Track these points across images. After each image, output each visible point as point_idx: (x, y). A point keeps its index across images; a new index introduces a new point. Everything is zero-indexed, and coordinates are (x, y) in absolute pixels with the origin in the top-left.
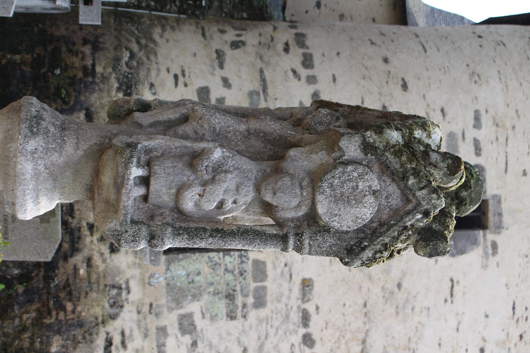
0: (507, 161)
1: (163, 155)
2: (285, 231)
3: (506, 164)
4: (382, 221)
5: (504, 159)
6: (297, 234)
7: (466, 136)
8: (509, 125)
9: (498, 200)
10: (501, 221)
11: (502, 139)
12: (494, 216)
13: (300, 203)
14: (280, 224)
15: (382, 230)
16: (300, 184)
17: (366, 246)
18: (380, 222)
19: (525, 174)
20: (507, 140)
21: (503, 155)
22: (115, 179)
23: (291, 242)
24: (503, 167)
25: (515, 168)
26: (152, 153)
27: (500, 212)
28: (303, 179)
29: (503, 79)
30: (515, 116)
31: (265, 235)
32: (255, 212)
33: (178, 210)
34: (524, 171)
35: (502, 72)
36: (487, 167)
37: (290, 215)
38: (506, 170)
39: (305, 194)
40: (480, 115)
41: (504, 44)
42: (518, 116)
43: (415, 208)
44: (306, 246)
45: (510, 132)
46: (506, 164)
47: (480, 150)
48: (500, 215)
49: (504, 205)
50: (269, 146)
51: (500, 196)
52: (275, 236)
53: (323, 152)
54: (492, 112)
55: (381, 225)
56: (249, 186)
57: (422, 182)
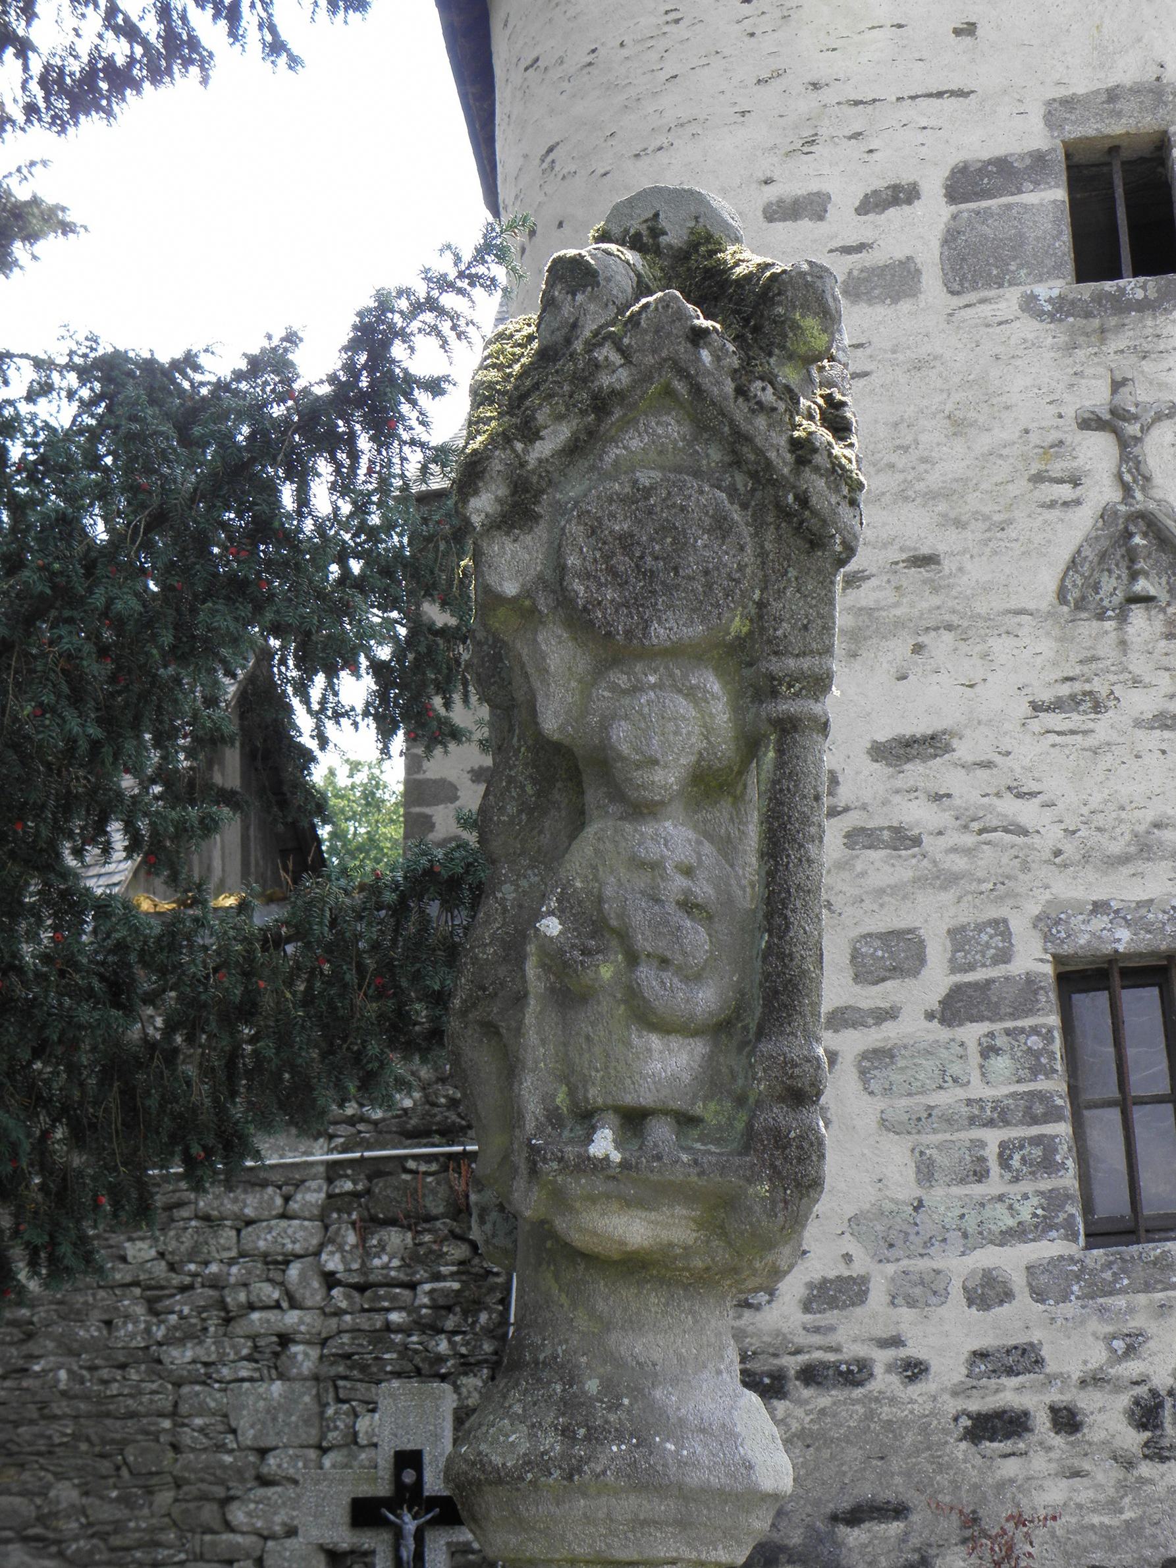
0: (930, 95)
1: (565, 1078)
2: (765, 727)
3: (940, 95)
4: (727, 459)
5: (923, 103)
6: (774, 694)
7: (852, 241)
8: (807, 104)
9: (1060, 109)
10: (1137, 90)
11: (857, 120)
12: (1119, 114)
13: (680, 691)
14: (751, 746)
15: (752, 457)
16: (625, 692)
17: (796, 497)
18: (730, 465)
19: (968, 30)
20: (857, 103)
21: (908, 111)
22: (628, 1205)
23: (786, 707)
24: (948, 103)
25: (952, 65)
26: (558, 1108)
27: (1104, 97)
28: (614, 688)
29: (662, 140)
30: (777, 85)
31: (779, 782)
32: (732, 820)
33: (721, 1029)
34: (957, 32)
35: (637, 148)
36: (955, 158)
37: (721, 713)
38: (961, 94)
39: (652, 679)
40: (781, 201)
41: (551, 150)
42: (778, 74)
43: (682, 373)
44: (806, 663)
45: (829, 96)
46: (940, 95)
47: (896, 188)
48: (1113, 95)
49: (1080, 86)
50: (556, 796)
51: (1049, 103)
52: (780, 752)
53: (540, 638)
54: (766, 165)
55: (737, 462)
56: (642, 834)
57: (606, 358)
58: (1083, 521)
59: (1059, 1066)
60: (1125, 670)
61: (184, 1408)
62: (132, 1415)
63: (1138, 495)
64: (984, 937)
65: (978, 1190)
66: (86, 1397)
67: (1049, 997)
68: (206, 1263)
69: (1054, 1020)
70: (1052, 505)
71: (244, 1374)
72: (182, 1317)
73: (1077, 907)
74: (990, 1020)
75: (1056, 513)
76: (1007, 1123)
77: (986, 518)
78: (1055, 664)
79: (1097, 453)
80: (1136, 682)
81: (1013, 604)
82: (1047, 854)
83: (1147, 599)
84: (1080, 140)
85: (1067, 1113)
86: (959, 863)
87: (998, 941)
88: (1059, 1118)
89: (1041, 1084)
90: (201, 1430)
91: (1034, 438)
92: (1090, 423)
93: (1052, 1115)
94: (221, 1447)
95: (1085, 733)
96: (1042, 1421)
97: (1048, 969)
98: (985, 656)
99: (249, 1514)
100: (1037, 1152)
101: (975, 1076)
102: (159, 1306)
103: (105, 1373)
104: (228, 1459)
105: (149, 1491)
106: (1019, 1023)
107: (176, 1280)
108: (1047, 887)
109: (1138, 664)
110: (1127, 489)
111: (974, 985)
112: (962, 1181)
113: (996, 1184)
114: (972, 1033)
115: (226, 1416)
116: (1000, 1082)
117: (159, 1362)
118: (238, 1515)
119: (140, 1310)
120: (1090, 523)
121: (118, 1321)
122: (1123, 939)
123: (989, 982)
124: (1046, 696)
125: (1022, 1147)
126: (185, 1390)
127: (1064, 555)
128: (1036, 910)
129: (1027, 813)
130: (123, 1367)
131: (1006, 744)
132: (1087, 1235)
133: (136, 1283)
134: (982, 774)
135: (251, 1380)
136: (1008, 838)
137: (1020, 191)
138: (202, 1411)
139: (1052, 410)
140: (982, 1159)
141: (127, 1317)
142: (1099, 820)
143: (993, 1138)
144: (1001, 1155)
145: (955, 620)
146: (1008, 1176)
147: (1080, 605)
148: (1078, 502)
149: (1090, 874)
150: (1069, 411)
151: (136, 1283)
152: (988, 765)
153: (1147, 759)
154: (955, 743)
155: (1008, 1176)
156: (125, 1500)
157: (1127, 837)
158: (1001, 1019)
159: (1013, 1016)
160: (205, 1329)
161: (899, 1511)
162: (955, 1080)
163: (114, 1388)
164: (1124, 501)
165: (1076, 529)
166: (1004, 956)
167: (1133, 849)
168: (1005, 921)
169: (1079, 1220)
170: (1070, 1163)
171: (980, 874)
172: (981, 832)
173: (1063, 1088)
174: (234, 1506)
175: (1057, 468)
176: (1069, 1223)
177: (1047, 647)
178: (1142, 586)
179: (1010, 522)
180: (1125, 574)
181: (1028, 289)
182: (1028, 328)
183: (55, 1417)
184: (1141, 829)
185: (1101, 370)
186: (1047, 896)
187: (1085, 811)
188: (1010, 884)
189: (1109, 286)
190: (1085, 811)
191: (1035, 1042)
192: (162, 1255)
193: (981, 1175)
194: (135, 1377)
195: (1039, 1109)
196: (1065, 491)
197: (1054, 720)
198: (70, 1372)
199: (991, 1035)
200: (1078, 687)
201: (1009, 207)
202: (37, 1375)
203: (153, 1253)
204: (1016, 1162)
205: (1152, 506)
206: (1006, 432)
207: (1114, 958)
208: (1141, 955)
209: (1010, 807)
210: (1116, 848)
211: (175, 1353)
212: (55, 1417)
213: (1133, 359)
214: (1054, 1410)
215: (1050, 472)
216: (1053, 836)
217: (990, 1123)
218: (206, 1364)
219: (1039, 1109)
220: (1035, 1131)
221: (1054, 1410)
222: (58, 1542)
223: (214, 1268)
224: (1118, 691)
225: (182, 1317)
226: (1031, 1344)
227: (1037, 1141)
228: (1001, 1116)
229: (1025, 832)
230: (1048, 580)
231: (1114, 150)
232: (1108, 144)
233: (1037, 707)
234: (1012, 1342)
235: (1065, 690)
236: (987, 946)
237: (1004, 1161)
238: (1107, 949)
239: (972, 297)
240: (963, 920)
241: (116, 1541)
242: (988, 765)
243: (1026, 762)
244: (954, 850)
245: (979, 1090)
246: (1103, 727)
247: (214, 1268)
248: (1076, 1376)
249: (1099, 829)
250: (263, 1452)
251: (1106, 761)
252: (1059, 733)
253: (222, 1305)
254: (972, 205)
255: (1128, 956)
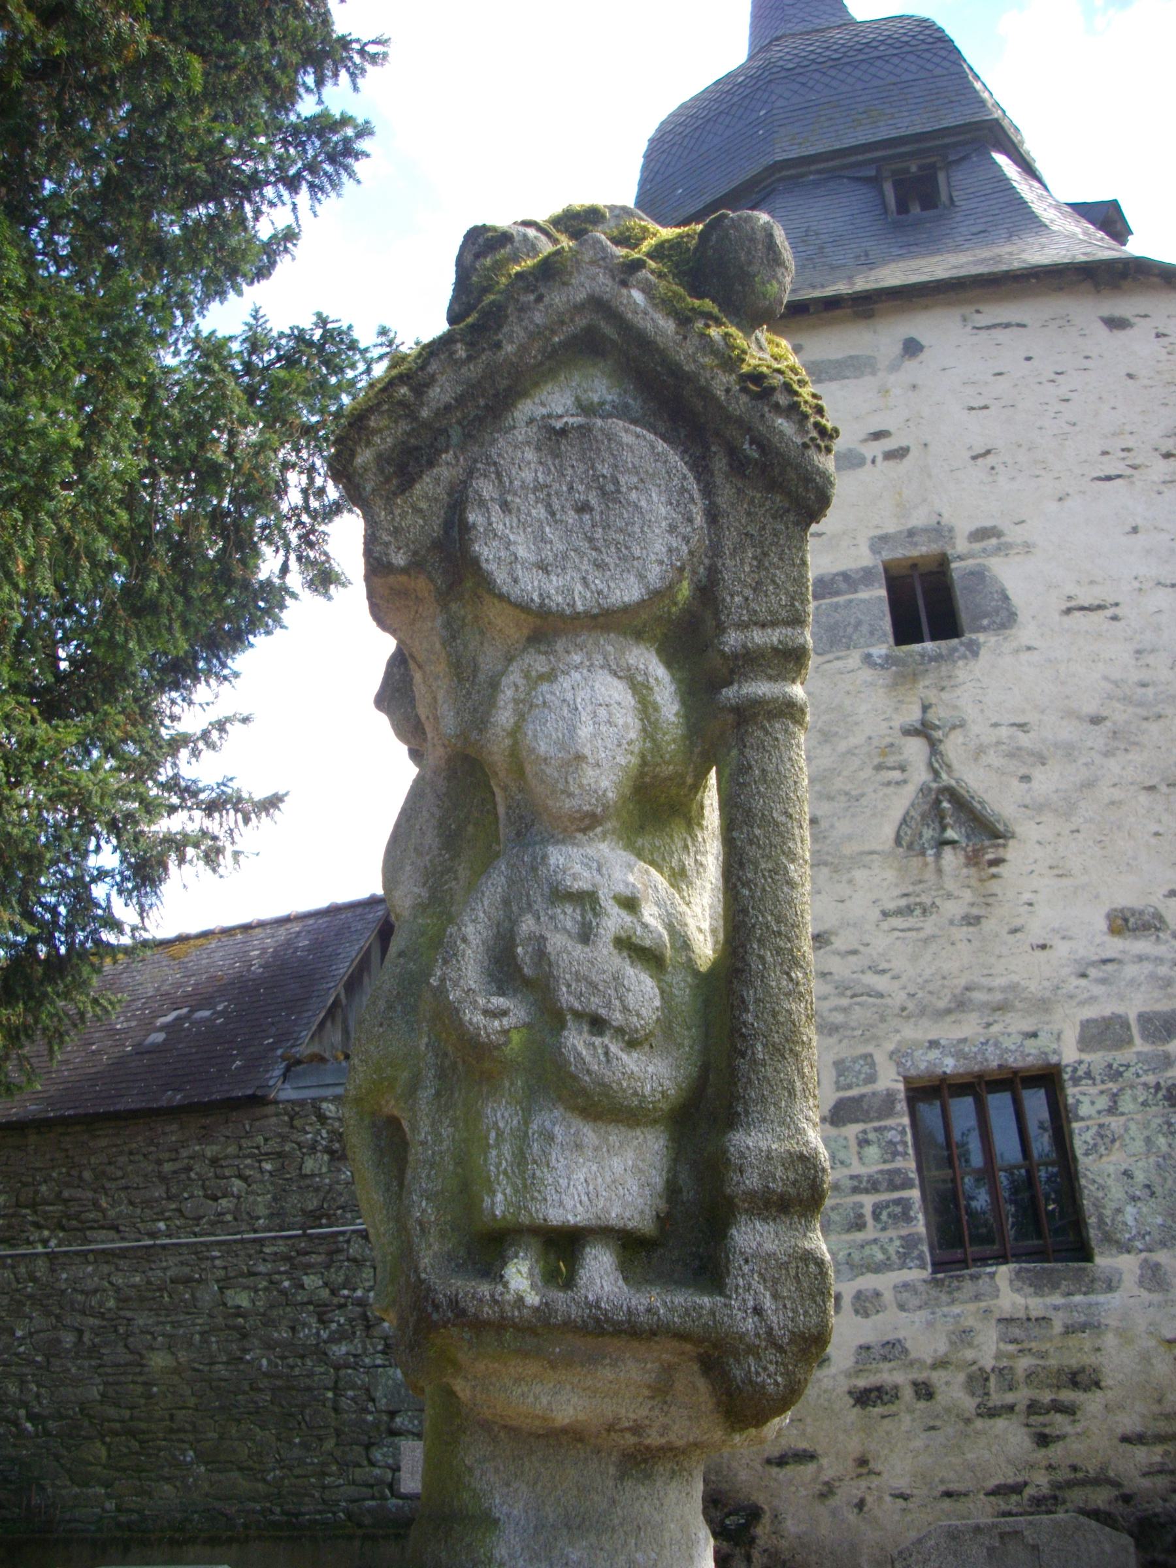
9: (880, 541)
10: (925, 530)
12: (916, 544)
48: (911, 533)
49: (891, 528)
51: (872, 538)
58: (909, 792)
59: (911, 1151)
60: (942, 888)
61: (341, 1384)
62: (309, 1389)
63: (944, 776)
64: (857, 1067)
65: (859, 1236)
66: (278, 1376)
67: (902, 1106)
68: (354, 1290)
69: (906, 1120)
70: (889, 784)
71: (379, 1362)
72: (339, 1325)
73: (916, 1044)
74: (864, 1121)
75: (891, 789)
76: (877, 1190)
77: (847, 794)
78: (897, 885)
79: (915, 749)
80: (949, 896)
81: (867, 848)
82: (897, 1011)
83: (952, 843)
84: (893, 560)
85: (917, 1182)
86: (839, 1018)
87: (866, 1069)
88: (912, 1186)
89: (899, 1163)
90: (353, 1399)
91: (875, 743)
92: (909, 732)
93: (907, 1184)
94: (366, 1410)
95: (918, 929)
96: (908, 1393)
97: (901, 1086)
98: (850, 881)
99: (384, 1455)
100: (898, 1210)
101: (855, 1161)
102: (326, 1317)
103: (291, 1361)
104: (370, 1418)
105: (320, 1439)
106: (882, 1123)
107: (335, 1300)
108: (898, 1031)
109: (950, 885)
110: (936, 774)
111: (852, 1099)
112: (848, 1231)
113: (870, 1232)
114: (852, 1130)
115: (368, 1390)
116: (872, 1163)
117: (326, 1354)
118: (377, 1455)
119: (313, 1321)
120: (913, 795)
121: (299, 1327)
122: (949, 1065)
123: (863, 1096)
124: (891, 906)
125: (887, 1206)
126: (342, 1372)
127: (897, 814)
128: (891, 1047)
129: (880, 983)
130: (303, 1357)
131: (867, 938)
132: (934, 1264)
133: (310, 1303)
134: (853, 959)
135: (384, 1366)
136: (871, 1000)
137: (856, 591)
138: (353, 1387)
139: (885, 724)
140: (861, 1216)
141: (304, 1325)
142: (930, 987)
143: (868, 1201)
144: (874, 1212)
145: (830, 859)
146: (879, 1226)
147: (910, 846)
148: (905, 782)
149: (925, 1022)
150: (896, 724)
151: (310, 1303)
152: (854, 952)
153: (959, 946)
154: (833, 939)
155: (879, 1226)
156: (305, 1446)
157: (949, 996)
158: (871, 1121)
159: (879, 1118)
160: (354, 1333)
161: (807, 1457)
162: (842, 1163)
163: (297, 1371)
164: (935, 781)
165: (901, 801)
166: (871, 1079)
167: (953, 1005)
168: (871, 1055)
169: (928, 1254)
170: (920, 1216)
171: (853, 1024)
172: (852, 997)
173: (912, 1165)
174: (373, 1449)
175: (891, 760)
176: (921, 1257)
177: (890, 875)
178: (950, 834)
179: (863, 795)
180: (937, 825)
181: (866, 650)
182: (867, 674)
183: (260, 1390)
184: (957, 991)
185: (915, 699)
186: (898, 1037)
187: (920, 980)
188: (874, 1030)
189: (917, 647)
190: (920, 980)
191: (890, 1135)
192: (326, 1284)
193: (859, 1225)
194: (309, 1363)
195: (898, 1181)
196: (896, 775)
197: (897, 922)
198: (269, 1360)
199: (865, 1132)
200: (912, 900)
201: (851, 601)
202: (248, 1362)
203: (321, 1283)
204: (884, 1217)
205: (953, 783)
206: (857, 739)
207: (944, 1079)
208: (961, 1075)
209: (871, 979)
210: (942, 1004)
211: (335, 1348)
212: (260, 1390)
213: (935, 691)
214: (915, 1384)
215: (886, 760)
216: (900, 998)
217: (866, 1191)
218: (355, 1356)
219: (898, 1181)
220: (896, 1195)
221: (915, 1384)
222: (263, 1471)
223: (359, 1293)
224: (938, 901)
225: (339, 1325)
226: (899, 1341)
227: (897, 1202)
228: (873, 1186)
229: (882, 996)
230: (888, 831)
231: (914, 566)
232: (910, 562)
233: (885, 914)
234: (886, 1338)
235: (903, 902)
236: (860, 1072)
237: (876, 1216)
238: (939, 1071)
239: (830, 656)
240: (843, 1055)
241: (298, 1471)
242: (854, 952)
243: (880, 950)
244: (835, 1009)
245: (857, 1169)
246: (929, 926)
247: (359, 1293)
248: (929, 1361)
249: (930, 993)
250: (392, 1414)
251: (933, 947)
252: (902, 930)
253: (365, 1317)
254: (827, 601)
255: (953, 1076)
